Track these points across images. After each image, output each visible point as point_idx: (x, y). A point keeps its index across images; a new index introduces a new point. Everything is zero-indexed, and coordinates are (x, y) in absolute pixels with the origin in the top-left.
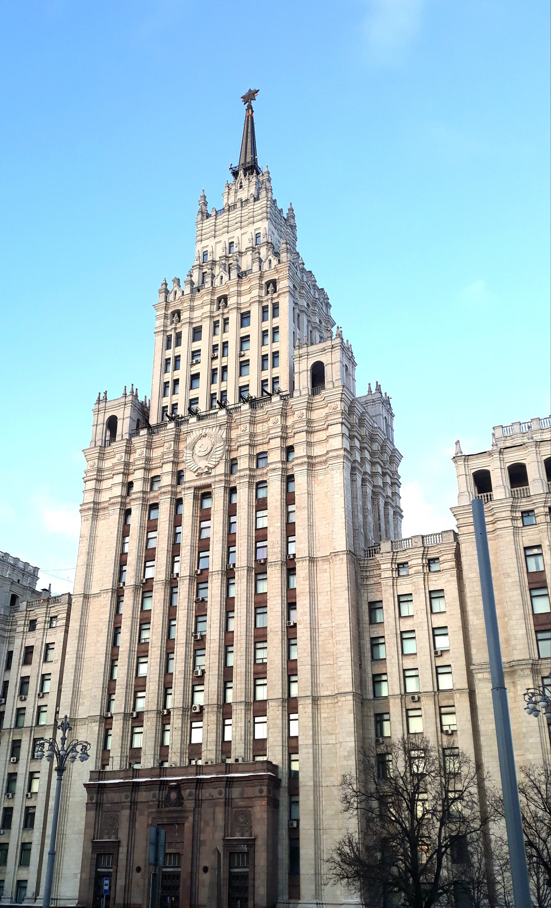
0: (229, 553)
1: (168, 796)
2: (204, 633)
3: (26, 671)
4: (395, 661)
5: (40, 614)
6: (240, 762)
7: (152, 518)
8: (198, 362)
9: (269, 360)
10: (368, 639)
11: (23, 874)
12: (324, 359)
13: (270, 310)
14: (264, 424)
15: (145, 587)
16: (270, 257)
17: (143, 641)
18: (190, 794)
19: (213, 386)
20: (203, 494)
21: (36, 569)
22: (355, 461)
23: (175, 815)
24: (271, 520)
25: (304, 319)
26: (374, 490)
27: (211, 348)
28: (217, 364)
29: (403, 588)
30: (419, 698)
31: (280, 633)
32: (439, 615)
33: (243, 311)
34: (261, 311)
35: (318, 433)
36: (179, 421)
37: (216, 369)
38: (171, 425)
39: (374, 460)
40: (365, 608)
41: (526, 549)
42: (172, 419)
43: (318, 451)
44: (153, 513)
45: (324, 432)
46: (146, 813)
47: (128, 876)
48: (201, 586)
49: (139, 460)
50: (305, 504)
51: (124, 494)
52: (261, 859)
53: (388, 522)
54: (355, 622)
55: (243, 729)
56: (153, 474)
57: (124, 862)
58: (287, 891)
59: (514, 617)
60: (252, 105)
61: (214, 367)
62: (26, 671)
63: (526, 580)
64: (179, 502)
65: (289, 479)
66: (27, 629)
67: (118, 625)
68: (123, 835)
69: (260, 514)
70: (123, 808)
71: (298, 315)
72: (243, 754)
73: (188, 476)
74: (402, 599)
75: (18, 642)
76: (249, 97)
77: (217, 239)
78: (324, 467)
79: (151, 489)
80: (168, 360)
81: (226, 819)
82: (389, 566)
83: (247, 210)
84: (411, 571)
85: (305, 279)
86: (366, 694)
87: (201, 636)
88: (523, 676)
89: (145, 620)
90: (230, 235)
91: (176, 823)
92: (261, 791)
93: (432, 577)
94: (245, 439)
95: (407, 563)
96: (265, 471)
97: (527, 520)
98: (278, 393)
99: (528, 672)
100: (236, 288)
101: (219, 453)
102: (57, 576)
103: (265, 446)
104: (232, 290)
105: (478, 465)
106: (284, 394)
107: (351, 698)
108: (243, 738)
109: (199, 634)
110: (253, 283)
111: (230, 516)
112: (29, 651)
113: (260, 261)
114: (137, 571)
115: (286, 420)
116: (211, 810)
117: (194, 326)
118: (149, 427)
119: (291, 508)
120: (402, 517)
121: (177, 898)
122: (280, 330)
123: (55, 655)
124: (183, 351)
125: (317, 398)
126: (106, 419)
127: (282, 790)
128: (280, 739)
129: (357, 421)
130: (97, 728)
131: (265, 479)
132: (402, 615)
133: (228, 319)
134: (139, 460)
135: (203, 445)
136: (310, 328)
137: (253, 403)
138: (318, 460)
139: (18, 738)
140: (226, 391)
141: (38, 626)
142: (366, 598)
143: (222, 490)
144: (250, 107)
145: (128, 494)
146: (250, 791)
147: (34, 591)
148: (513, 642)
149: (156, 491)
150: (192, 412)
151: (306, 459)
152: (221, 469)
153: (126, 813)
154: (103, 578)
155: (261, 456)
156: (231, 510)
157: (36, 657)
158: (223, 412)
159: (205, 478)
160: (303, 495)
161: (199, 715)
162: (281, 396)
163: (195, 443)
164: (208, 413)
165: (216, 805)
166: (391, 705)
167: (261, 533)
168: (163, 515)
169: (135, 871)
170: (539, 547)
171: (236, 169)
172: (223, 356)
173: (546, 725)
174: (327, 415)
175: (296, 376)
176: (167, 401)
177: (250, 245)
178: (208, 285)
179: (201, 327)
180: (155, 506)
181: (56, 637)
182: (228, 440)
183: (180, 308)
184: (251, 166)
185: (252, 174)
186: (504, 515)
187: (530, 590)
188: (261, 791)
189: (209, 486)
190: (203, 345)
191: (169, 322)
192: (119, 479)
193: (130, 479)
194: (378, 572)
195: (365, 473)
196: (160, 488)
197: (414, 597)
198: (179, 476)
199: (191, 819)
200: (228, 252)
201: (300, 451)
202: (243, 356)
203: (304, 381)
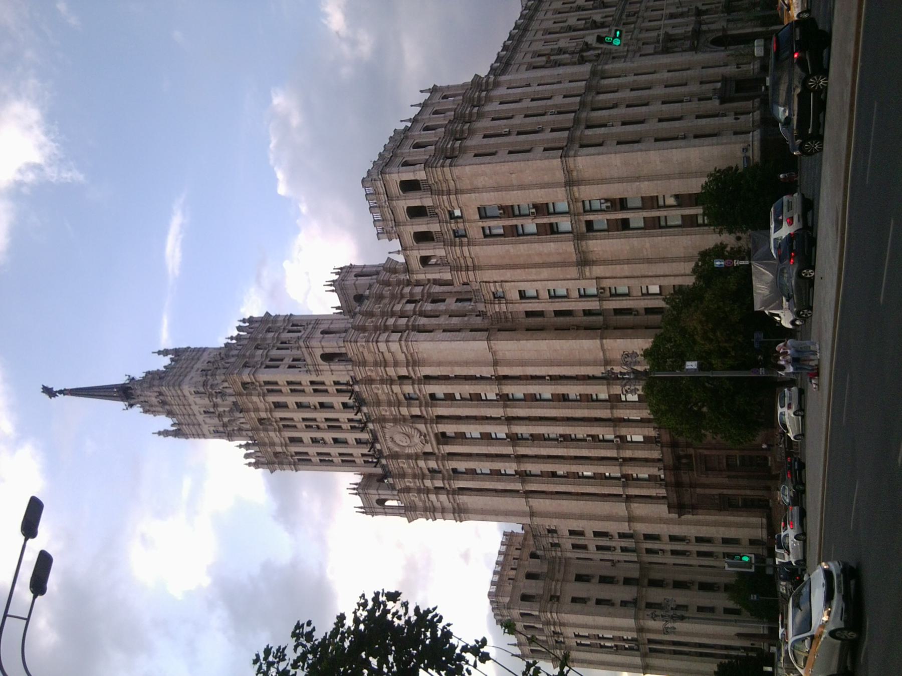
3: (592, 547)
8: (323, 439)
9: (318, 388)
12: (318, 352)
13: (272, 387)
15: (505, 399)
20: (443, 438)
30: (602, 288)
43: (401, 357)
49: (409, 465)
50: (449, 368)
60: (58, 389)
62: (592, 547)
64: (455, 471)
68: (715, 492)
73: (428, 449)
75: (569, 555)
82: (497, 306)
88: (587, 246)
89: (532, 399)
99: (584, 243)
100: (252, 413)
104: (253, 416)
107: (604, 341)
114: (501, 445)
121: (758, 457)
124: (312, 450)
130: (636, 505)
135: (400, 439)
138: (410, 358)
139: (644, 551)
144: (61, 392)
145: (440, 472)
148: (561, 251)
151: (410, 368)
153: (699, 491)
154: (519, 503)
155: (409, 398)
157: (580, 541)
161: (623, 438)
170: (483, 228)
180: (433, 396)
186: (458, 251)
189: (436, 435)
191: (285, 460)
192: (433, 497)
198: (427, 455)
199: (701, 451)
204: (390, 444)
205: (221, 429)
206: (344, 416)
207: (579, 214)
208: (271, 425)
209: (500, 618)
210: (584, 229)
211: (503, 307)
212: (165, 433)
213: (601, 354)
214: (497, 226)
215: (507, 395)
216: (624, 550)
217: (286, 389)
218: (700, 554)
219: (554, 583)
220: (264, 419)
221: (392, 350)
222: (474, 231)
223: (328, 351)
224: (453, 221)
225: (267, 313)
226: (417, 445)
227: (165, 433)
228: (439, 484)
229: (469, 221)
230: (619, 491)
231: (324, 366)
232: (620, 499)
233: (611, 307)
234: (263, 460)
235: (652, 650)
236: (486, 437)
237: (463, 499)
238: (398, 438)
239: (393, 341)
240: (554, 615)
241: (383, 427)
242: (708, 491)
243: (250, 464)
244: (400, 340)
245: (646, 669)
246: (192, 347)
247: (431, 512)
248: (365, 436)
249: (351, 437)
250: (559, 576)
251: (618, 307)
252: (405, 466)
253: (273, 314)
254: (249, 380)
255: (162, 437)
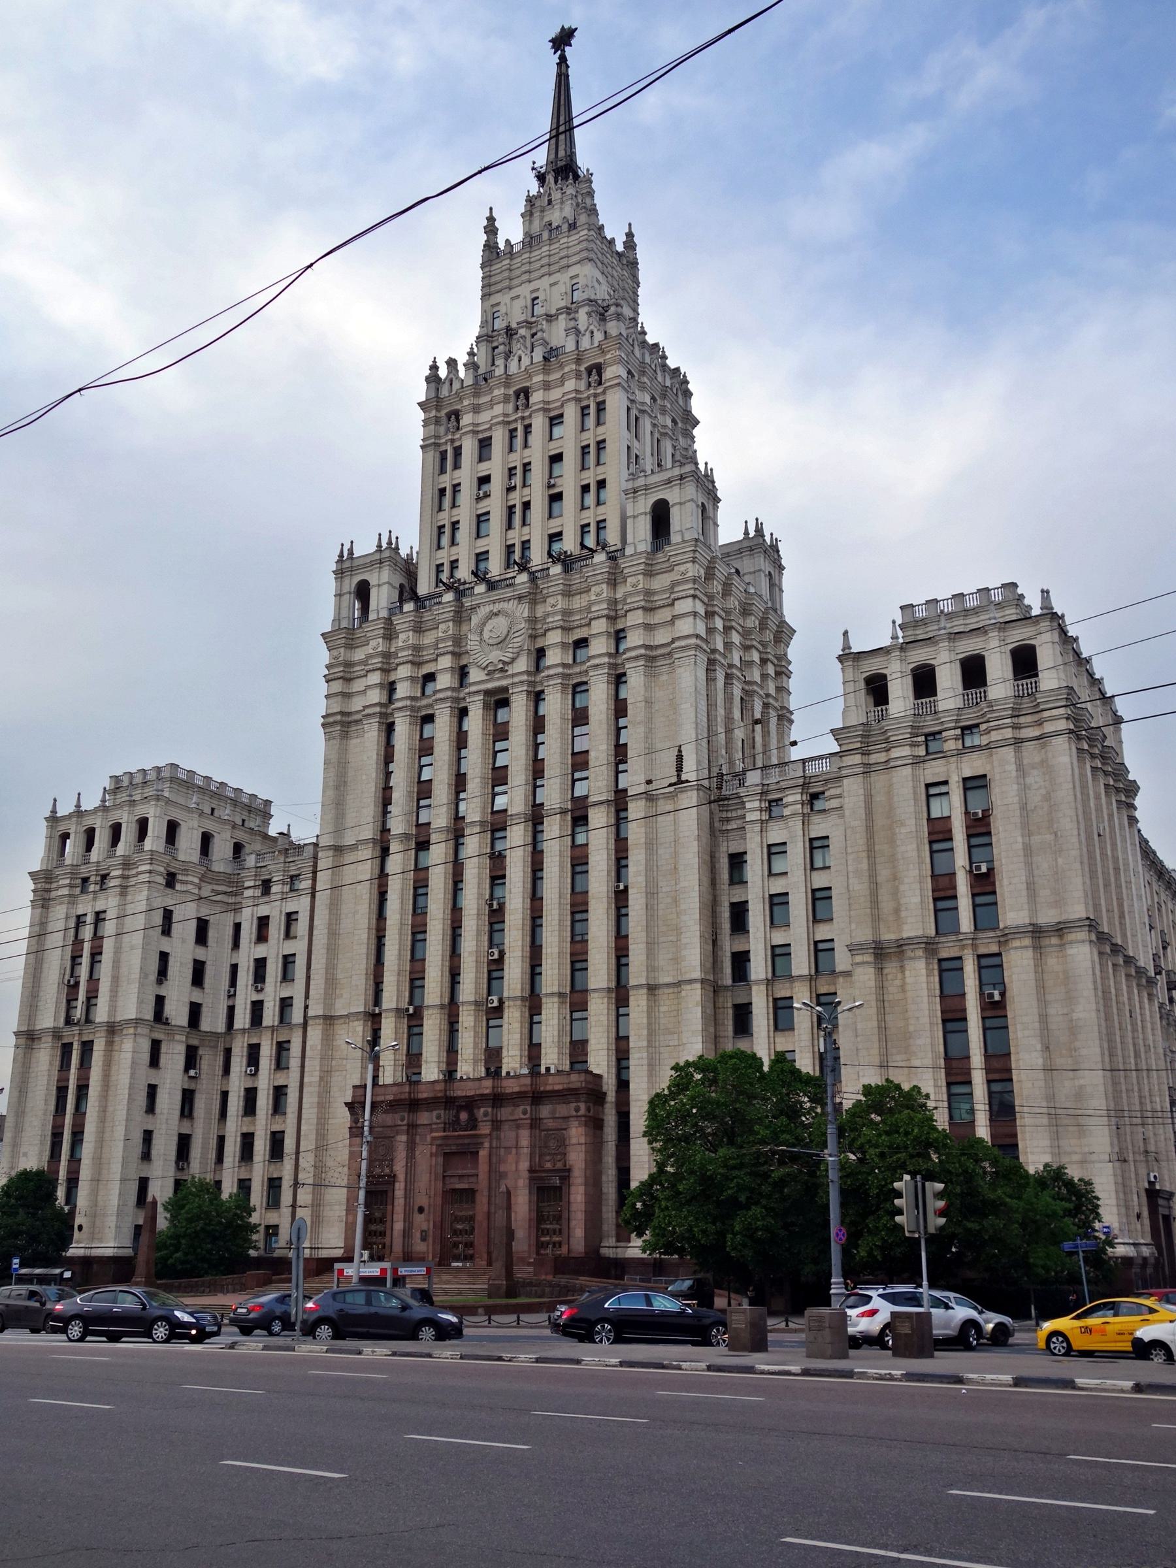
0: (535, 787)
1: (457, 1117)
2: (502, 901)
4: (761, 934)
5: (276, 870)
6: (552, 1071)
7: (425, 736)
8: (487, 495)
10: (727, 904)
11: (272, 1218)
12: (672, 496)
14: (583, 596)
16: (592, 327)
17: (419, 911)
18: (486, 1115)
19: (511, 533)
20: (499, 700)
21: (268, 803)
22: (714, 651)
23: (466, 1141)
24: (596, 741)
25: (646, 424)
26: (747, 688)
27: (506, 471)
28: (516, 498)
29: (776, 834)
31: (605, 900)
32: (821, 872)
33: (552, 414)
34: (579, 415)
35: (660, 611)
36: (460, 591)
37: (514, 506)
38: (449, 597)
39: (748, 643)
40: (724, 863)
41: (928, 786)
42: (449, 587)
44: (428, 729)
45: (669, 608)
46: (429, 1138)
47: (408, 1219)
48: (498, 835)
49: (403, 649)
50: (641, 717)
51: (384, 700)
52: (578, 1195)
53: (769, 732)
54: (706, 881)
55: (556, 1028)
56: (427, 669)
57: (402, 1201)
58: (614, 1233)
59: (906, 880)
60: (567, 54)
61: (511, 503)
63: (926, 829)
64: (463, 713)
65: (619, 679)
66: (258, 892)
67: (383, 889)
68: (399, 1168)
69: (577, 731)
70: (398, 1133)
71: (637, 419)
72: (556, 1061)
73: (475, 675)
74: (774, 850)
76: (563, 39)
77: (513, 293)
78: (668, 662)
79: (423, 693)
80: (442, 492)
81: (532, 1146)
83: (557, 245)
84: (787, 812)
85: (647, 360)
86: (722, 979)
87: (499, 904)
90: (533, 286)
91: (469, 1153)
92: (577, 1110)
93: (815, 819)
94: (557, 618)
95: (781, 799)
96: (584, 668)
97: (933, 746)
98: (603, 549)
99: (920, 953)
101: (520, 640)
102: (299, 817)
103: (584, 629)
105: (872, 666)
106: (612, 549)
108: (556, 1039)
109: (495, 903)
110: (567, 369)
111: (535, 735)
112: (263, 922)
113: (578, 332)
115: (615, 590)
116: (512, 1134)
117: (481, 436)
118: (415, 597)
119: (622, 722)
120: (791, 722)
122: (608, 444)
123: (301, 927)
124: (466, 475)
125: (660, 555)
126: (353, 586)
127: (608, 1106)
128: (604, 1040)
129: (720, 588)
131: (584, 679)
132: (774, 872)
133: (530, 425)
134: (403, 649)
135: (499, 625)
136: (656, 435)
137: (567, 562)
139: (254, 1041)
140: (529, 541)
141: (275, 889)
142: (725, 849)
143: (524, 696)
144: (563, 60)
146: (563, 1110)
147: (266, 836)
148: (903, 914)
149: (430, 696)
150: (479, 575)
152: (522, 664)
154: (362, 824)
156: (538, 725)
157: (275, 930)
158: (523, 578)
159: (499, 679)
160: (638, 705)
162: (608, 553)
163: (484, 624)
164: (503, 577)
165: (518, 1127)
166: (754, 993)
167: (579, 759)
168: (442, 731)
169: (426, 1208)
170: (946, 783)
171: (543, 170)
172: (524, 486)
173: (940, 1021)
174: (674, 584)
175: (629, 522)
176: (443, 557)
177: (563, 304)
178: (499, 371)
179: (490, 438)
180: (429, 719)
181: (300, 905)
182: (533, 620)
183: (459, 407)
184: (566, 166)
185: (567, 178)
187: (931, 842)
188: (577, 1110)
189: (505, 689)
190: (495, 467)
191: (442, 430)
192: (375, 678)
193: (392, 678)
194: (740, 812)
195: (731, 666)
196: (435, 692)
197: (789, 848)
199: (487, 1145)
200: (530, 315)
201: (634, 639)
202: (554, 486)
203: (641, 532)
204: (484, 611)
205: (499, 324)
206: (537, 534)
207: (974, 947)
208: (448, 430)
209: (126, 783)
210: (944, 954)
211: (755, 816)
212: (491, 229)
213: (667, 979)
214: (953, 807)
215: (626, 810)
216: (257, 1008)
217: (516, 459)
218: (247, 1140)
219: (196, 880)
220: (458, 421)
221: (369, 692)
222: (86, 907)
223: (675, 513)
224: (99, 878)
225: (697, 422)
226: (483, 657)
227: (491, 229)
228: (402, 690)
229: (94, 899)
230: (390, 999)
231: (645, 505)
232: (371, 1003)
233: (755, 1000)
234: (445, 392)
235: (67, 1049)
236: (499, 776)
237: (371, 734)
238: (499, 625)
239: (695, 624)
240: (145, 877)
241: (520, 598)
242: (401, 1155)
243: (434, 367)
244: (697, 636)
245: (28, 1038)
246: (640, 291)
247: (342, 674)
248: (495, 567)
249: (494, 544)
250: (206, 891)
251: (262, 1053)
252: (369, 650)
253: (696, 432)
254: (532, 400)
255: (485, 223)
